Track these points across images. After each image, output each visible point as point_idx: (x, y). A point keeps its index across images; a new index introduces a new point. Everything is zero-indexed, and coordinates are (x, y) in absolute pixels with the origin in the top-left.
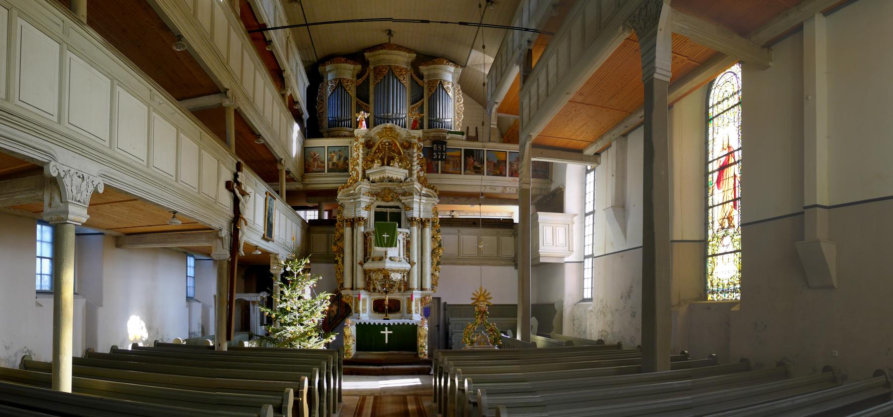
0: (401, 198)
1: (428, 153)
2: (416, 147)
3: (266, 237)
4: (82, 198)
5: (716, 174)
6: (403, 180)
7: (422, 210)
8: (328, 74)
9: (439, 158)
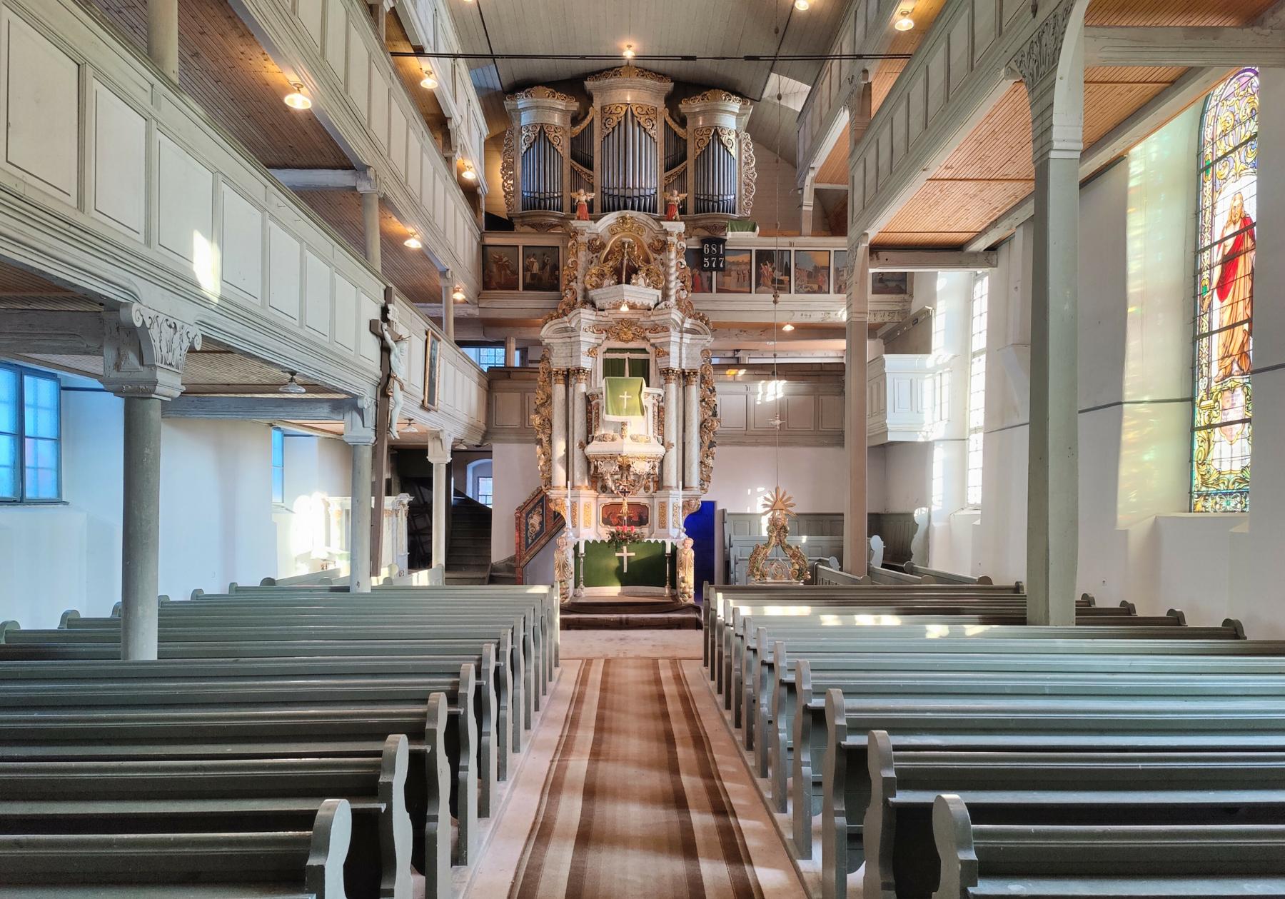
0: (648, 334)
1: (695, 258)
2: (673, 250)
3: (427, 404)
4: (174, 360)
5: (1217, 272)
6: (653, 307)
7: (684, 356)
8: (520, 115)
9: (714, 266)
